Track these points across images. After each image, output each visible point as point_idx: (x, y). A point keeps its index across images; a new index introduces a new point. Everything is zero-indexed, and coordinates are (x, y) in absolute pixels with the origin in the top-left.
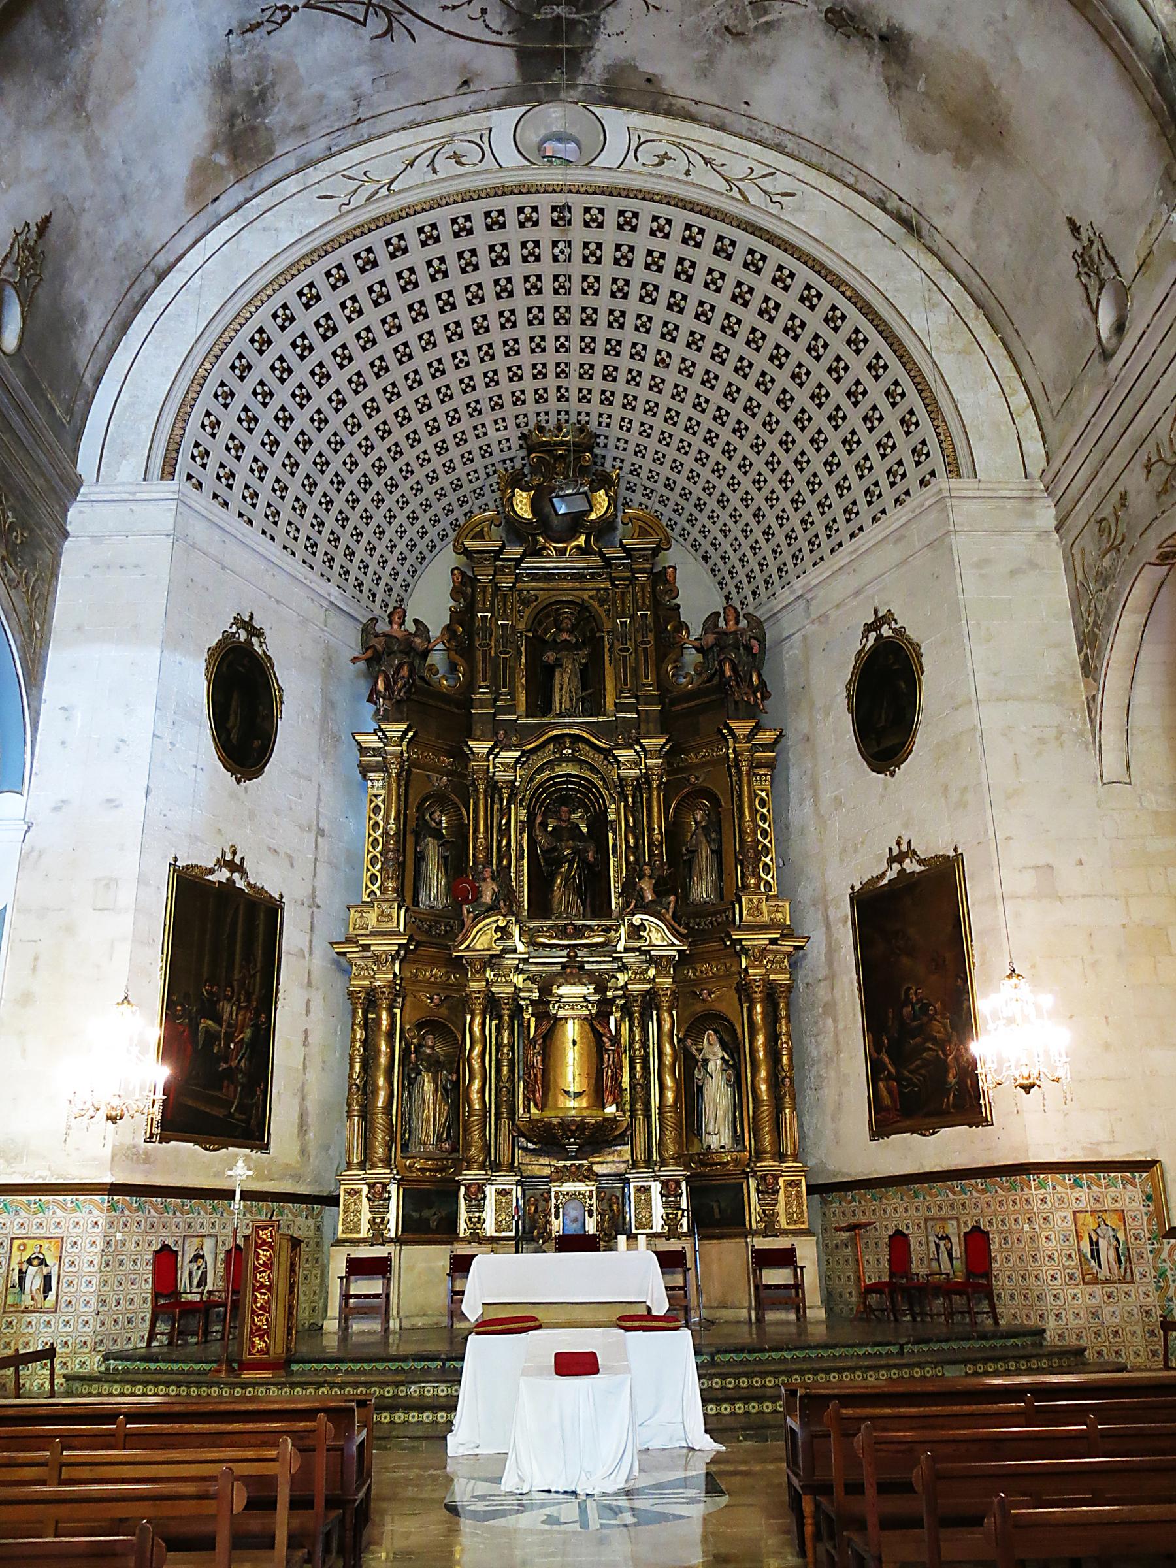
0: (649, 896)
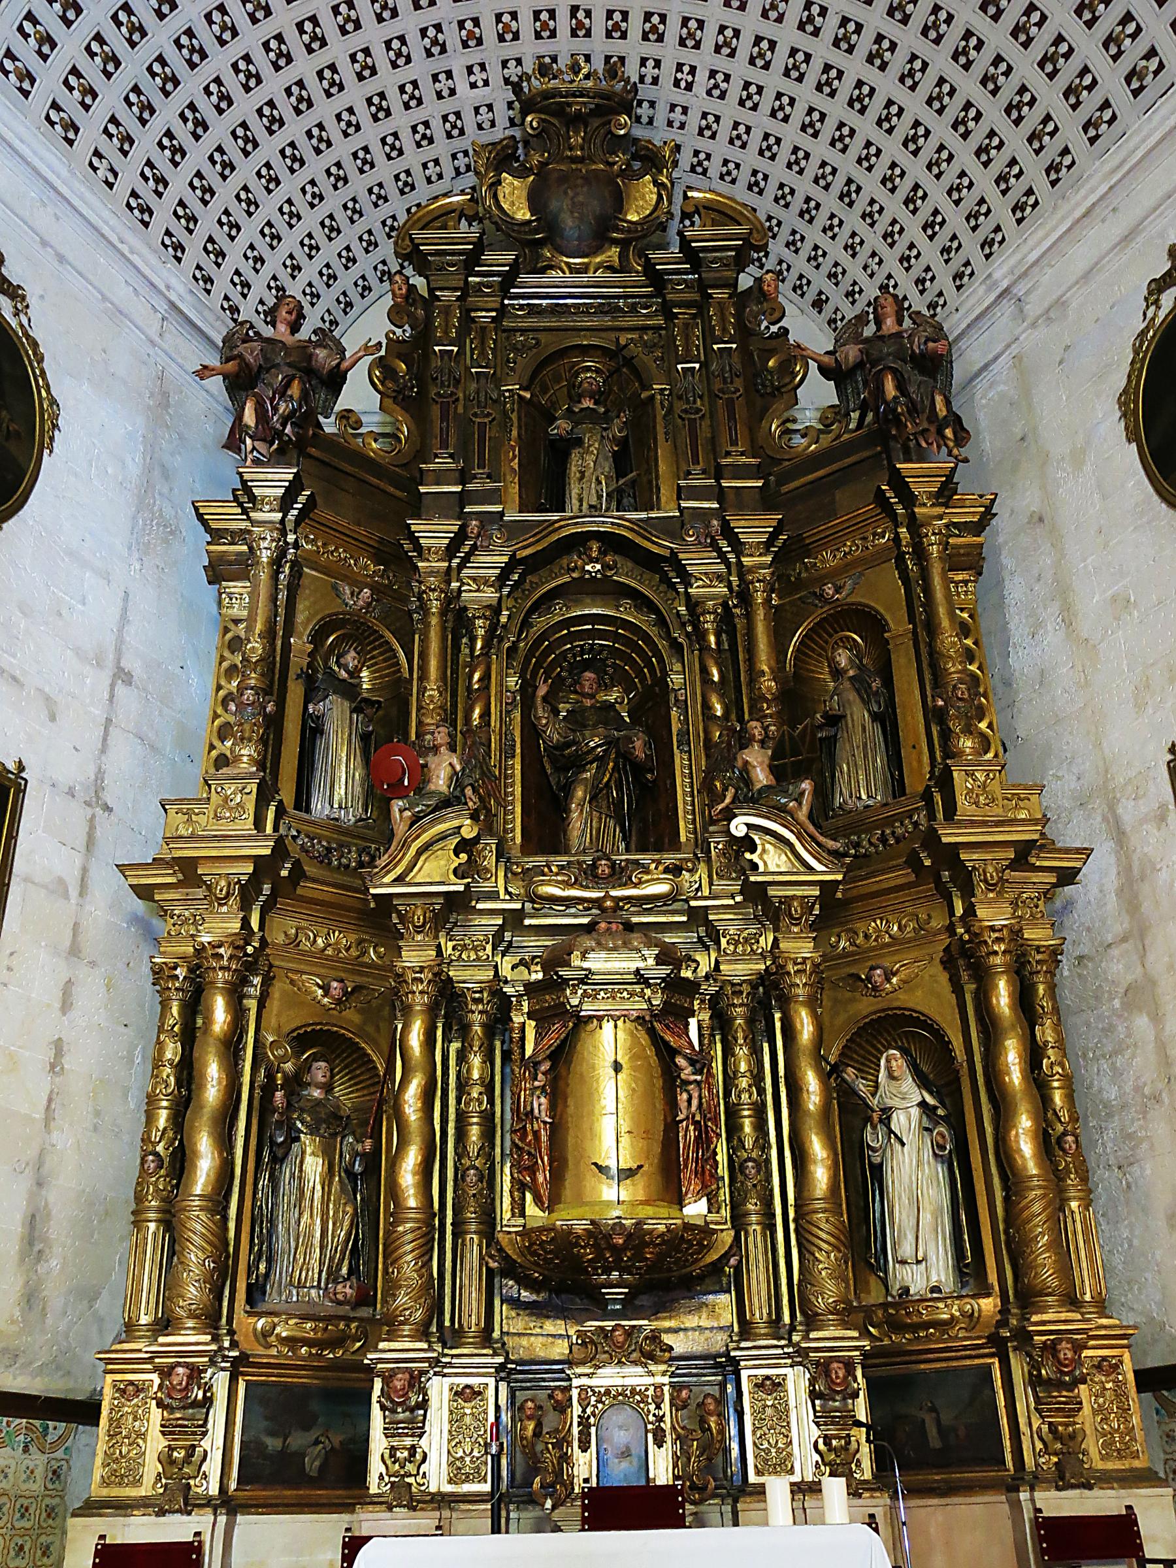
0: (761, 777)
